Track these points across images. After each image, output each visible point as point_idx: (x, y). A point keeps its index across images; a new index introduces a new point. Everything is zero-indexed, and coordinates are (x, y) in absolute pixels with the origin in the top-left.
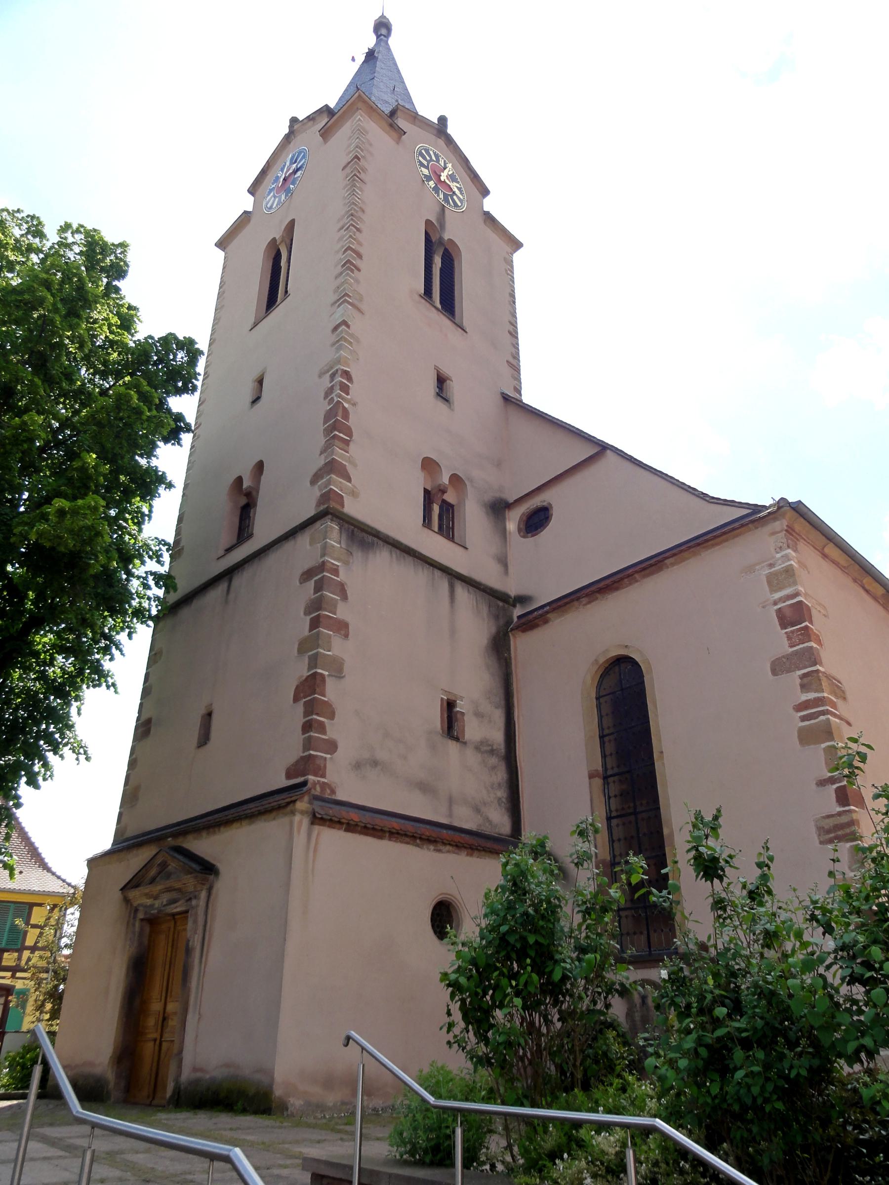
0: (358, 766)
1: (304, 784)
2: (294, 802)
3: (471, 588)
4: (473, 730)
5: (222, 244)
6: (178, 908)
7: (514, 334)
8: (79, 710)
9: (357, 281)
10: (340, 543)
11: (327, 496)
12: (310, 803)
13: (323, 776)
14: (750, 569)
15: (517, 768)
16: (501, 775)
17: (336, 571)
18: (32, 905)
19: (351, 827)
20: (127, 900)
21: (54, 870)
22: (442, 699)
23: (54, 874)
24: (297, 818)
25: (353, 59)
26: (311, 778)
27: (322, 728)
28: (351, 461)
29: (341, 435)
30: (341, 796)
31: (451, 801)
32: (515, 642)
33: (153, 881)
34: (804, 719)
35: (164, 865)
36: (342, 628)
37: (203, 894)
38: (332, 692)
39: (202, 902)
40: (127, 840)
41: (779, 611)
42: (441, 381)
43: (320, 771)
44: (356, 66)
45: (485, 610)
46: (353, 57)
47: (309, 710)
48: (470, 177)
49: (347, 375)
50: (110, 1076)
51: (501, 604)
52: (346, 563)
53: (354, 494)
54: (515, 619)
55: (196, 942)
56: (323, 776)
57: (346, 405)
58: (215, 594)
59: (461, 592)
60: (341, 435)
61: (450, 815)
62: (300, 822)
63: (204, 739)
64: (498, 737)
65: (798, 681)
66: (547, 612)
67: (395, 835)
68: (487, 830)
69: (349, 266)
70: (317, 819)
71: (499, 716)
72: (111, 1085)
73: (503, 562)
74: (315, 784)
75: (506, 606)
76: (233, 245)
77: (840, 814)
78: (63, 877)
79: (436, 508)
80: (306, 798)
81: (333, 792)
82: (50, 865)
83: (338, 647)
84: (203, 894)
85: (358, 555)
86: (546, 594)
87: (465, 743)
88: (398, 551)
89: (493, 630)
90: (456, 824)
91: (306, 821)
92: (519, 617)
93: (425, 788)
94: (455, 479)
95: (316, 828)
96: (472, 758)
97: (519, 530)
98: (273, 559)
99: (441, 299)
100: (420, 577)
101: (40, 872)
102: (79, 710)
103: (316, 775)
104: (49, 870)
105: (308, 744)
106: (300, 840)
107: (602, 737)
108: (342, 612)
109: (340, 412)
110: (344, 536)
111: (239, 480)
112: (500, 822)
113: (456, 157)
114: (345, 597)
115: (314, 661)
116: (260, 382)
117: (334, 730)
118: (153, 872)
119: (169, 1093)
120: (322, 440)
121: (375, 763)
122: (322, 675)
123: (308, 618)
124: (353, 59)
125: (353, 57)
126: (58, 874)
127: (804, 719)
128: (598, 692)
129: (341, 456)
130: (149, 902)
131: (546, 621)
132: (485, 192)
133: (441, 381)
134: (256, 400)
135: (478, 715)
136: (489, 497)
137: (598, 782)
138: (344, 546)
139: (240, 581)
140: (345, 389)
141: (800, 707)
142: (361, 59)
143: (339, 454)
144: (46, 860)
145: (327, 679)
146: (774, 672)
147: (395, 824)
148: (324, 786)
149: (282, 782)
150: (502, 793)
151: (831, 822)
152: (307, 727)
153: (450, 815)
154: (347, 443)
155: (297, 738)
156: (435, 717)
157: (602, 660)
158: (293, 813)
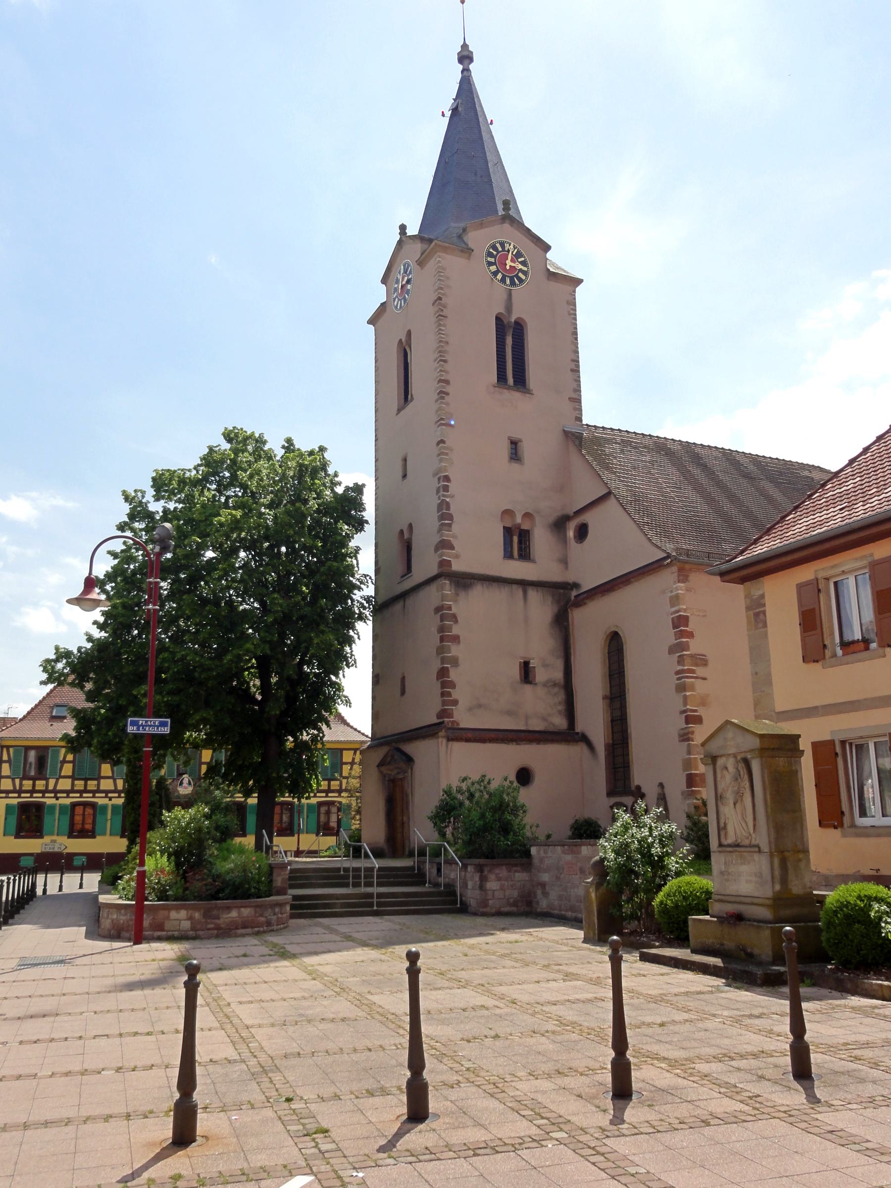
0: (470, 709)
1: (443, 723)
2: (438, 733)
3: (539, 589)
4: (541, 675)
5: (372, 321)
6: (400, 776)
7: (576, 371)
8: (343, 675)
9: (448, 404)
10: (451, 591)
11: (443, 563)
12: (446, 731)
13: (452, 718)
14: (664, 592)
15: (572, 691)
16: (562, 696)
17: (450, 608)
18: (341, 750)
19: (468, 740)
20: (381, 772)
21: (351, 724)
22: (520, 662)
23: (352, 727)
24: (440, 740)
25: (443, 115)
26: (446, 720)
27: (449, 694)
28: (455, 537)
29: (446, 522)
30: (462, 726)
31: (527, 717)
32: (572, 613)
33: (389, 763)
34: (678, 679)
35: (393, 756)
36: (456, 639)
37: (410, 771)
38: (453, 675)
39: (410, 774)
40: (378, 739)
41: (673, 618)
42: (514, 444)
43: (450, 715)
44: (446, 120)
45: (549, 599)
46: (443, 112)
47: (444, 685)
48: (533, 242)
49: (447, 479)
50: (385, 847)
51: (562, 591)
52: (456, 601)
53: (457, 556)
54: (573, 598)
55: (409, 791)
56: (452, 718)
57: (448, 500)
58: (398, 607)
59: (532, 593)
60: (446, 522)
61: (527, 724)
62: (442, 741)
63: (403, 692)
64: (559, 675)
65: (676, 659)
66: (584, 599)
67: (491, 740)
68: (551, 729)
69: (442, 394)
70: (449, 739)
71: (560, 664)
72: (386, 851)
73: (564, 562)
74: (448, 722)
75: (566, 591)
76: (380, 322)
77: (686, 728)
78: (358, 729)
79: (515, 539)
80: (443, 730)
81: (458, 724)
82: (348, 721)
83: (455, 650)
84: (410, 771)
85: (462, 594)
86: (587, 585)
87: (536, 684)
88: (487, 583)
89: (556, 610)
90: (531, 729)
91: (445, 741)
92: (576, 597)
93: (510, 713)
94: (527, 515)
95: (450, 743)
96: (540, 691)
97: (575, 537)
98: (422, 594)
99: (514, 374)
100: (500, 595)
101: (342, 727)
102: (343, 675)
103: (448, 718)
104: (348, 725)
105: (444, 703)
106: (443, 749)
107: (610, 676)
108: (456, 630)
109: (445, 506)
110: (453, 585)
111: (402, 532)
112: (560, 722)
113: (520, 232)
114: (456, 621)
115: (443, 660)
116: (405, 460)
117: (456, 694)
118: (389, 759)
119: (407, 853)
120: (437, 524)
121: (480, 706)
122: (447, 668)
123: (439, 635)
124: (443, 115)
125: (443, 112)
126: (355, 727)
127: (678, 679)
128: (609, 649)
129: (448, 536)
130: (389, 772)
131: (585, 604)
132: (547, 248)
133: (514, 444)
134: (405, 476)
135: (545, 666)
136: (552, 519)
137: (608, 701)
138: (453, 591)
139: (410, 601)
140: (446, 489)
141: (678, 673)
142: (448, 114)
143: (446, 535)
144: (345, 718)
145: (450, 669)
146: (669, 653)
147: (492, 735)
148: (453, 722)
149: (435, 720)
150: (561, 708)
151: (682, 732)
152: (443, 694)
153: (527, 724)
154: (450, 525)
155: (438, 700)
156: (515, 672)
157: (608, 633)
158: (438, 738)
